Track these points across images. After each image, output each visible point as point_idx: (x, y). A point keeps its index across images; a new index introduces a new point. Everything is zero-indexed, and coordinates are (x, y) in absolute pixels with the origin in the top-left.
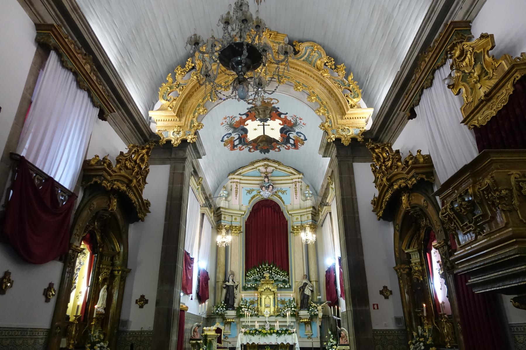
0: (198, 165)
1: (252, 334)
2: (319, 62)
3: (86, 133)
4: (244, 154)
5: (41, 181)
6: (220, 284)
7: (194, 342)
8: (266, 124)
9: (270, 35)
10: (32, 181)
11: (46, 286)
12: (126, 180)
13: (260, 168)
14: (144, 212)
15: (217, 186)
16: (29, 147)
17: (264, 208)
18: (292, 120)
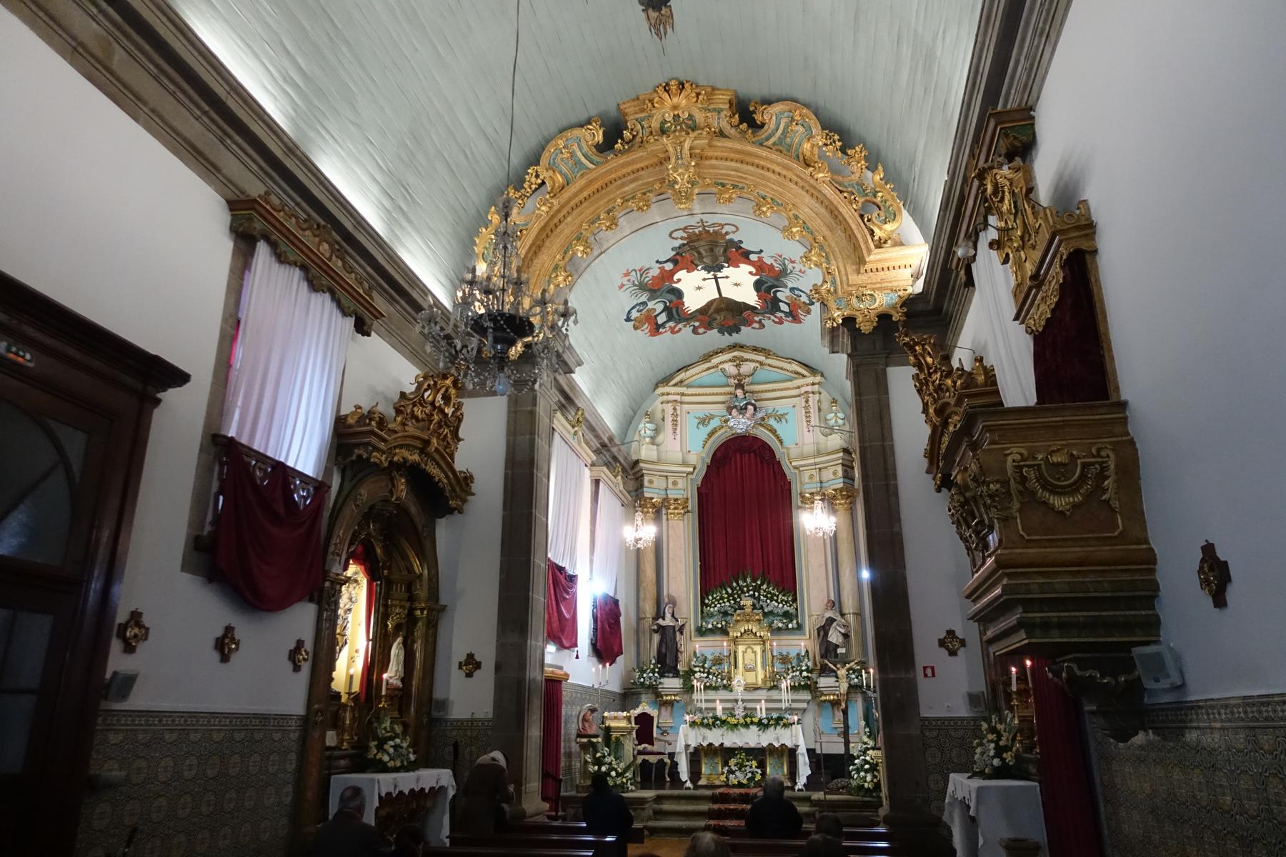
0: (573, 385)
1: (708, 726)
2: (807, 146)
3: (334, 370)
4: (684, 340)
5: (265, 470)
6: (648, 623)
7: (585, 740)
8: (719, 275)
9: (698, 95)
10: (251, 477)
11: (292, 646)
12: (418, 444)
13: (726, 366)
14: (462, 495)
15: (631, 413)
16: (243, 403)
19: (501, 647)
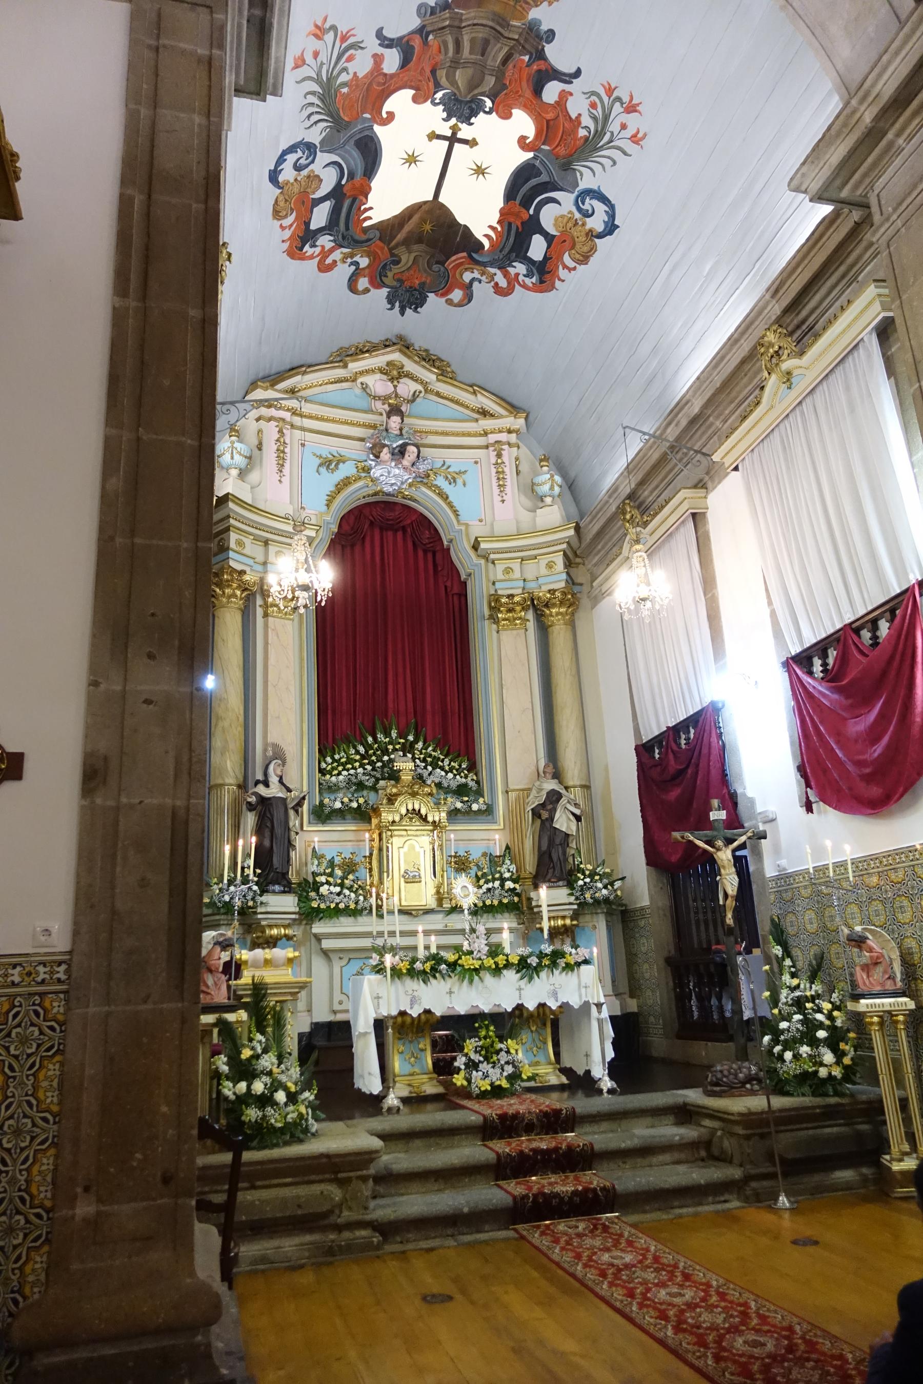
1: (424, 976)
13: (370, 380)
18: (586, 121)
19: (108, 709)
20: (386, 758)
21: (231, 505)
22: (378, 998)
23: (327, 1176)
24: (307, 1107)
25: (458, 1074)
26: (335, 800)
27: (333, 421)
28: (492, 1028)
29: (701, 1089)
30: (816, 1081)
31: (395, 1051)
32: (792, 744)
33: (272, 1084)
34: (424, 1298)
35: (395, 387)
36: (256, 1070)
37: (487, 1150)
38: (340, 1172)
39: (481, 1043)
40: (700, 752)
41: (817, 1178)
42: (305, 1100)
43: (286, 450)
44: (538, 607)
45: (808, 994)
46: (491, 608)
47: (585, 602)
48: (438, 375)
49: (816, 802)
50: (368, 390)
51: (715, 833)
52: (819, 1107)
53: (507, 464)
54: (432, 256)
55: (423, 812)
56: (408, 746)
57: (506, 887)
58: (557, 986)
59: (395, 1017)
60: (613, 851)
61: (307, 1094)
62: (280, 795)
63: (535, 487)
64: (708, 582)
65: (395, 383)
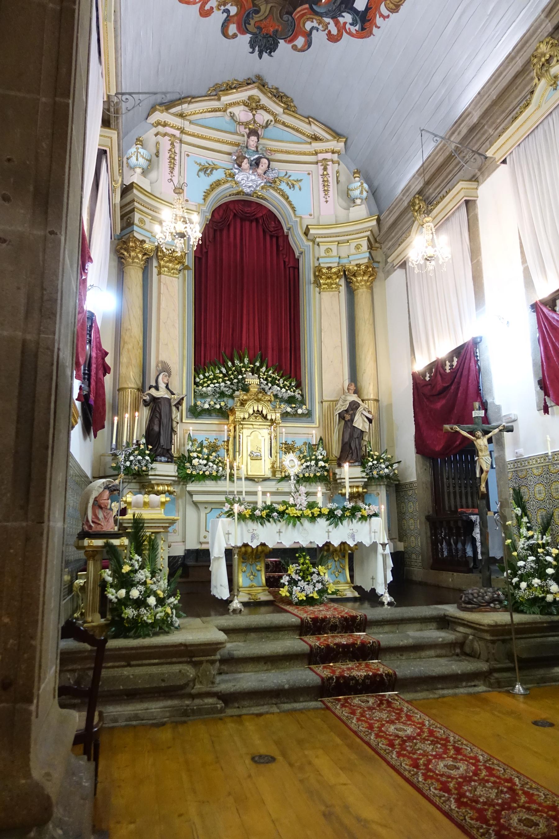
1: (261, 520)
7: (99, 542)
17: (238, 221)
20: (240, 377)
21: (135, 191)
22: (229, 534)
23: (184, 659)
24: (172, 609)
25: (283, 587)
26: (205, 403)
27: (209, 139)
28: (308, 558)
29: (456, 605)
30: (543, 604)
31: (240, 571)
32: (534, 365)
33: (145, 592)
34: (253, 759)
35: (254, 115)
36: (134, 581)
37: (303, 643)
38: (194, 657)
39: (300, 568)
40: (462, 372)
41: (541, 672)
42: (171, 603)
43: (176, 158)
44: (348, 276)
45: (540, 542)
46: (315, 276)
47: (381, 275)
48: (284, 109)
49: (551, 406)
50: (235, 118)
51: (476, 426)
52: (546, 622)
53: (331, 175)
54: (283, 7)
55: (264, 413)
56: (255, 369)
57: (319, 465)
58: (354, 530)
59: (240, 548)
60: (392, 443)
61: (172, 599)
62: (166, 396)
63: (350, 193)
64: (475, 252)
65: (254, 112)
